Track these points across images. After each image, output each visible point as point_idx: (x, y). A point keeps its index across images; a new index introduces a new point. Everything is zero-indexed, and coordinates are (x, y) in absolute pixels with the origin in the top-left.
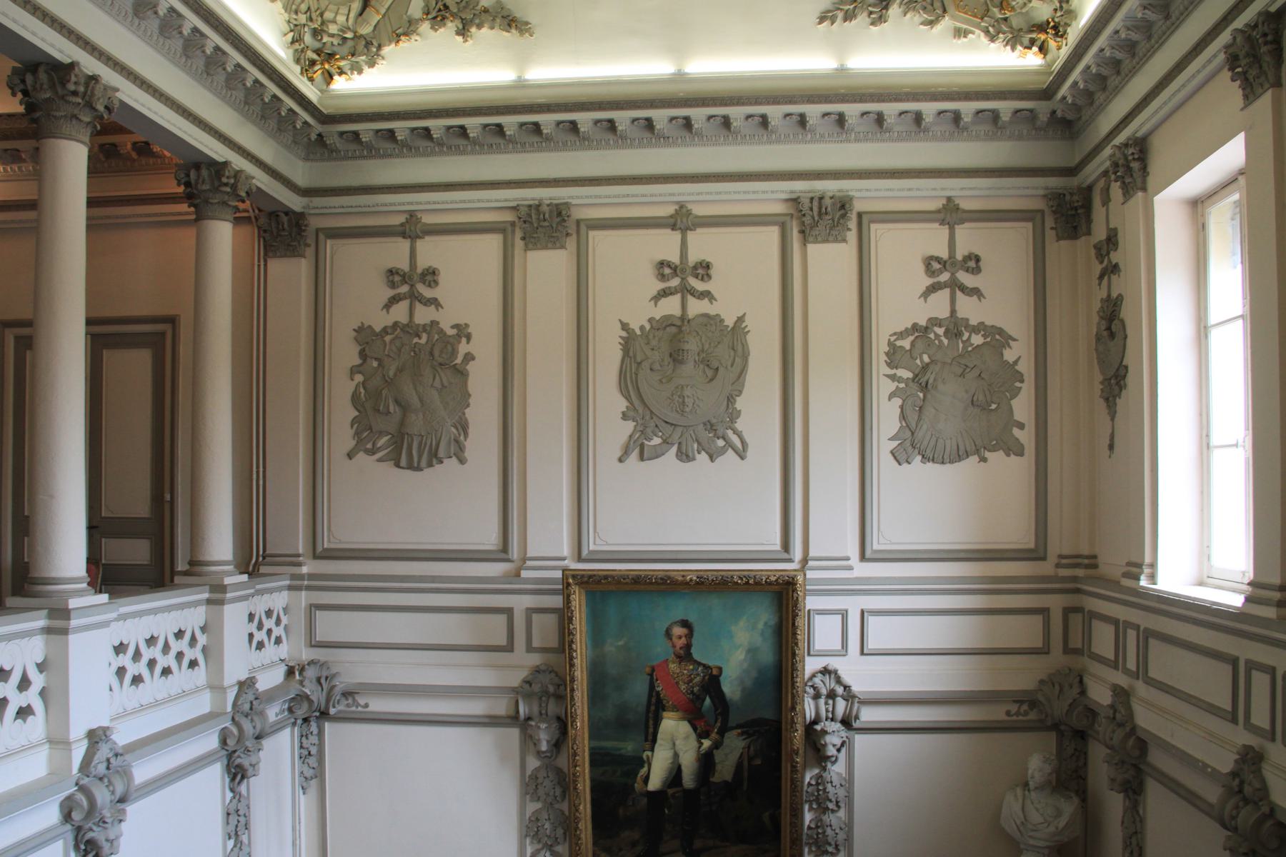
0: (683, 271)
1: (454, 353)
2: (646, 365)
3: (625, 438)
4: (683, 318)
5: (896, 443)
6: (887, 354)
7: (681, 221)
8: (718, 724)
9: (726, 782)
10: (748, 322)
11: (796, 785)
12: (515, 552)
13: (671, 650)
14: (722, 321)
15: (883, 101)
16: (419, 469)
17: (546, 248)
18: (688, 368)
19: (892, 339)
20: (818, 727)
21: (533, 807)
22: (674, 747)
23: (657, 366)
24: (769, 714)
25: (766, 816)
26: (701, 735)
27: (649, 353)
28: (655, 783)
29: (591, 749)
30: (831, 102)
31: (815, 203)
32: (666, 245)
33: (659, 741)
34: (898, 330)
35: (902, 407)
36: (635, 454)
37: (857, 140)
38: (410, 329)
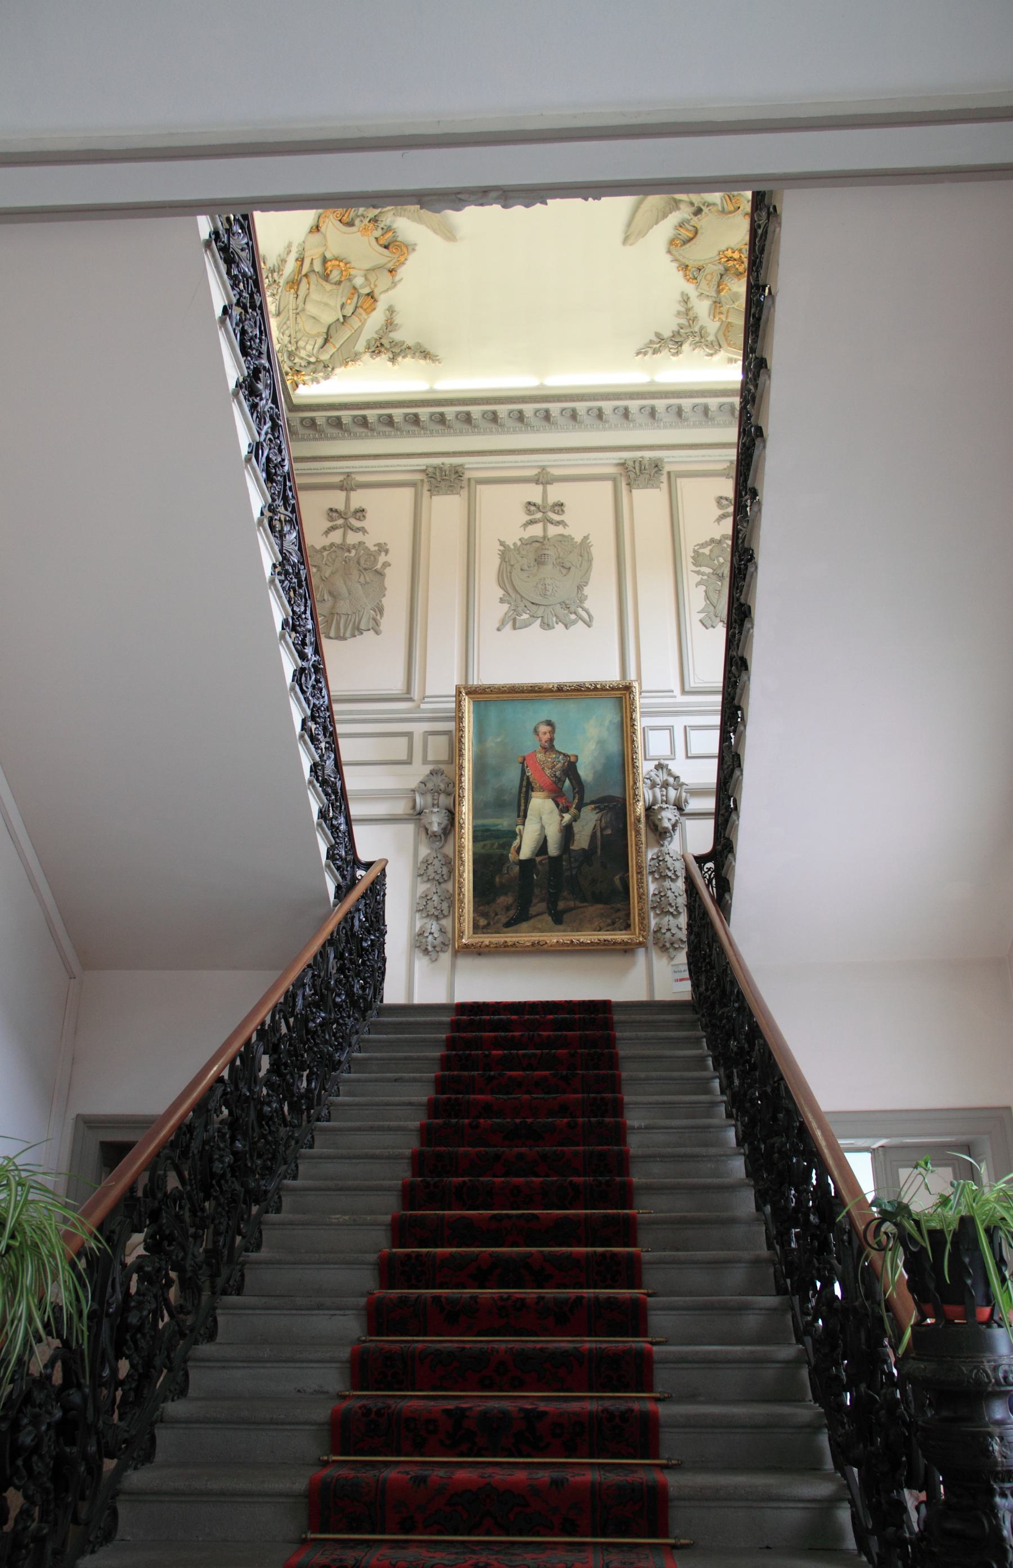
0: (544, 507)
1: (376, 561)
4: (544, 537)
5: (703, 615)
7: (543, 479)
8: (576, 801)
10: (591, 539)
12: (416, 694)
13: (538, 743)
16: (344, 638)
17: (446, 494)
18: (548, 569)
20: (656, 807)
21: (422, 888)
22: (541, 822)
23: (525, 567)
24: (616, 792)
25: (617, 879)
28: (525, 853)
29: (474, 827)
30: (645, 398)
32: (534, 493)
35: (706, 592)
36: (509, 625)
37: (665, 427)
38: (344, 547)
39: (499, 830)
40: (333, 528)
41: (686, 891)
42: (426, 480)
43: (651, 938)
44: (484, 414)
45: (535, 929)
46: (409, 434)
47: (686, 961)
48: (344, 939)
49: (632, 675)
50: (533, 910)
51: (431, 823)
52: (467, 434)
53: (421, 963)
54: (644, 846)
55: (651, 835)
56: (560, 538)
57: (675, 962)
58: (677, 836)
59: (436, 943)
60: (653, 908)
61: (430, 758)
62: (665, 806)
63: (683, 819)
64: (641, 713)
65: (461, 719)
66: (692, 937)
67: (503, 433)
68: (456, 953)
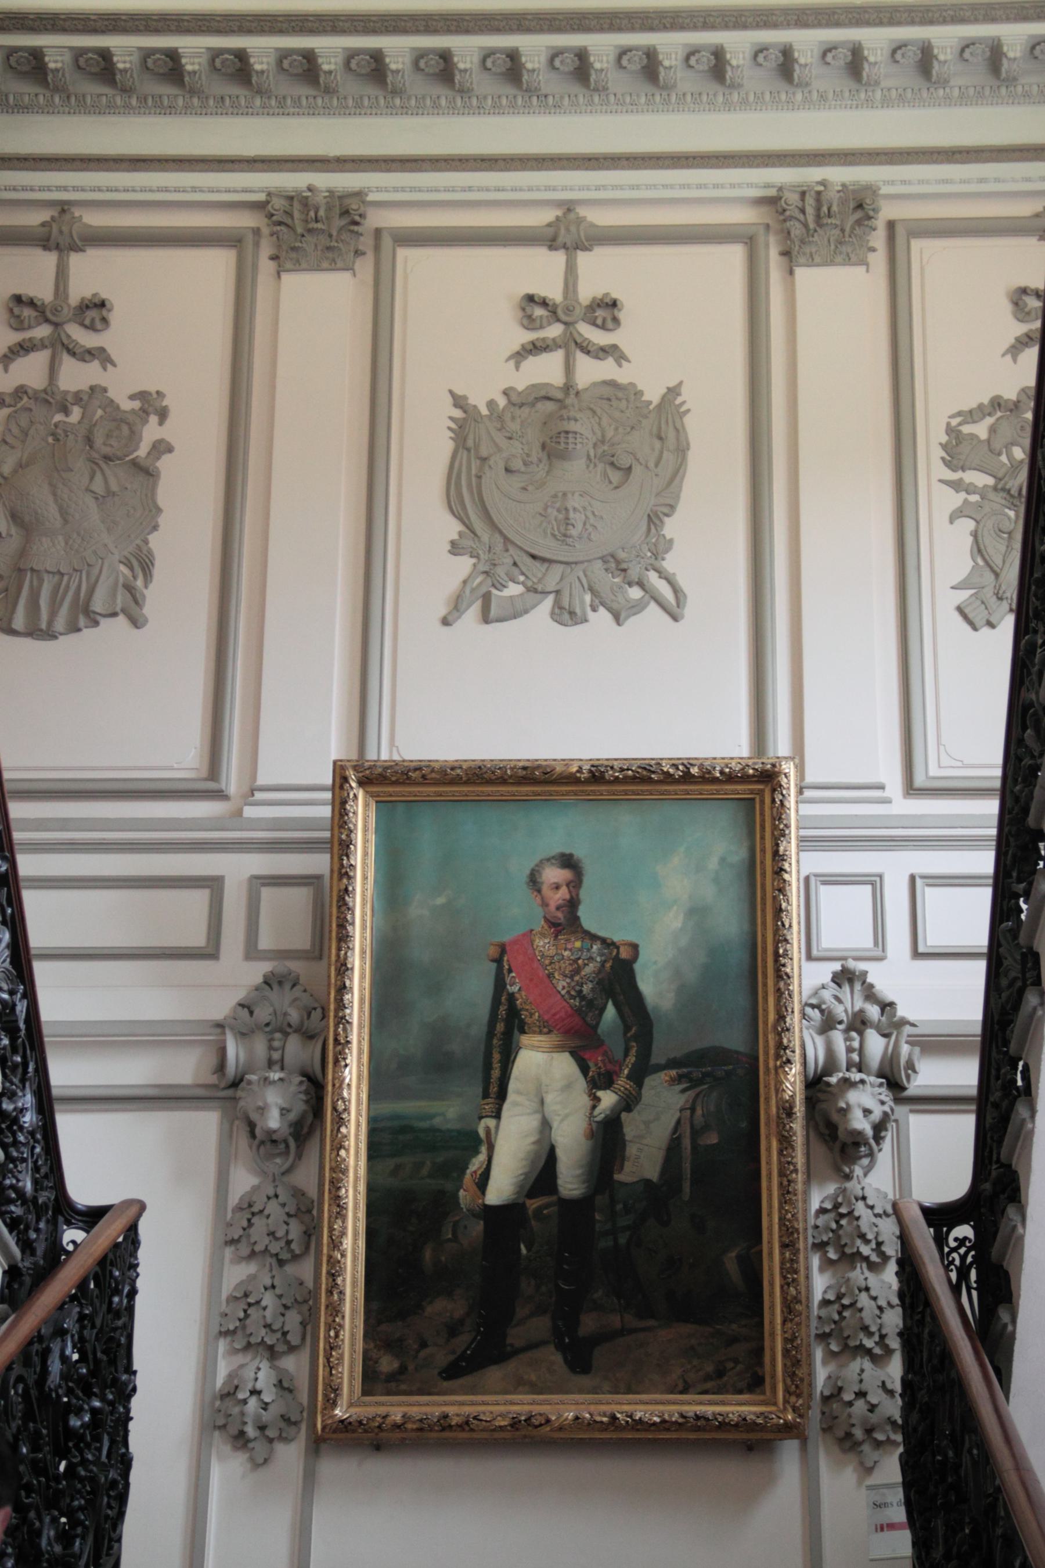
0: (569, 310)
1: (134, 437)
2: (498, 463)
3: (453, 584)
5: (964, 595)
6: (944, 447)
7: (567, 236)
8: (631, 1059)
9: (648, 1182)
10: (686, 394)
12: (232, 781)
13: (539, 912)
14: (641, 393)
15: (931, 22)
16: (50, 635)
17: (319, 269)
18: (575, 470)
19: (954, 422)
20: (833, 1080)
21: (237, 1274)
22: (542, 1110)
23: (517, 464)
24: (734, 1040)
26: (599, 1081)
27: (503, 443)
28: (500, 1189)
30: (838, 24)
31: (810, 201)
32: (542, 272)
33: (511, 1096)
34: (966, 408)
35: (975, 535)
36: (473, 612)
37: (886, 103)
38: (51, 399)
39: (434, 1130)
40: (23, 349)
41: (901, 1295)
42: (265, 231)
43: (815, 1414)
44: (419, 56)
45: (519, 1384)
46: (224, 107)
47: (899, 1478)
48: (19, 1409)
49: (781, 745)
50: (515, 1336)
51: (262, 1110)
52: (374, 110)
53: (226, 1470)
54: (800, 1177)
55: (820, 1150)
56: (607, 391)
57: (877, 1478)
58: (885, 1155)
59: (266, 1417)
60: (823, 1337)
61: (265, 943)
62: (855, 1076)
63: (901, 1111)
64: (801, 840)
65: (342, 847)
66: (915, 1416)
67: (468, 110)
68: (317, 1444)
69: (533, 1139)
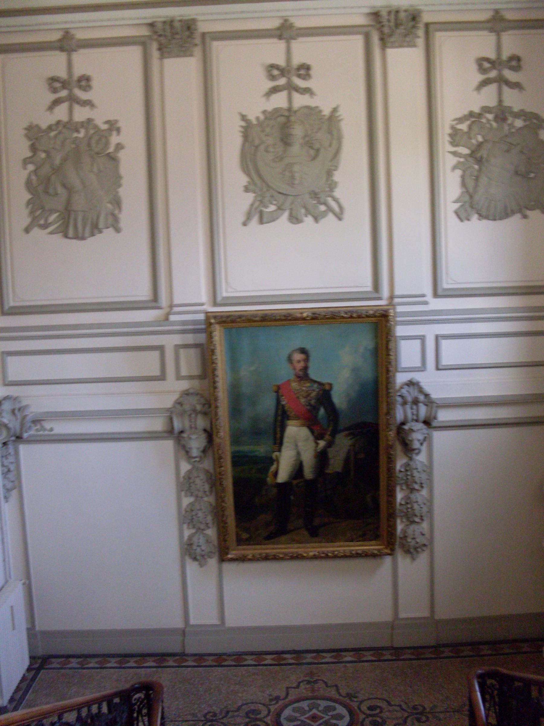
1: (107, 144)
4: (289, 109)
5: (457, 205)
6: (450, 135)
8: (330, 428)
9: (338, 473)
11: (390, 471)
12: (164, 301)
14: (320, 111)
16: (83, 238)
21: (187, 501)
22: (296, 449)
24: (369, 419)
26: (318, 437)
28: (282, 477)
32: (274, 52)
35: (463, 177)
36: (255, 219)
38: (70, 126)
40: (56, 102)
45: (293, 541)
69: (293, 459)
